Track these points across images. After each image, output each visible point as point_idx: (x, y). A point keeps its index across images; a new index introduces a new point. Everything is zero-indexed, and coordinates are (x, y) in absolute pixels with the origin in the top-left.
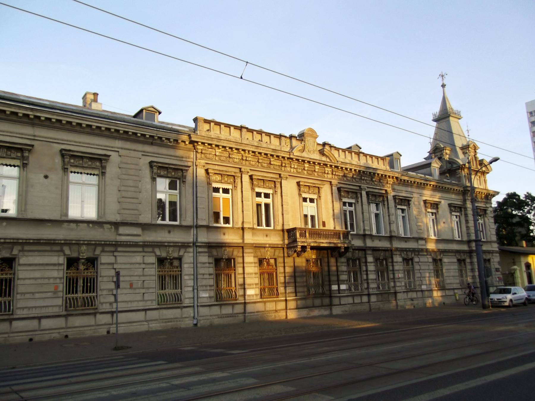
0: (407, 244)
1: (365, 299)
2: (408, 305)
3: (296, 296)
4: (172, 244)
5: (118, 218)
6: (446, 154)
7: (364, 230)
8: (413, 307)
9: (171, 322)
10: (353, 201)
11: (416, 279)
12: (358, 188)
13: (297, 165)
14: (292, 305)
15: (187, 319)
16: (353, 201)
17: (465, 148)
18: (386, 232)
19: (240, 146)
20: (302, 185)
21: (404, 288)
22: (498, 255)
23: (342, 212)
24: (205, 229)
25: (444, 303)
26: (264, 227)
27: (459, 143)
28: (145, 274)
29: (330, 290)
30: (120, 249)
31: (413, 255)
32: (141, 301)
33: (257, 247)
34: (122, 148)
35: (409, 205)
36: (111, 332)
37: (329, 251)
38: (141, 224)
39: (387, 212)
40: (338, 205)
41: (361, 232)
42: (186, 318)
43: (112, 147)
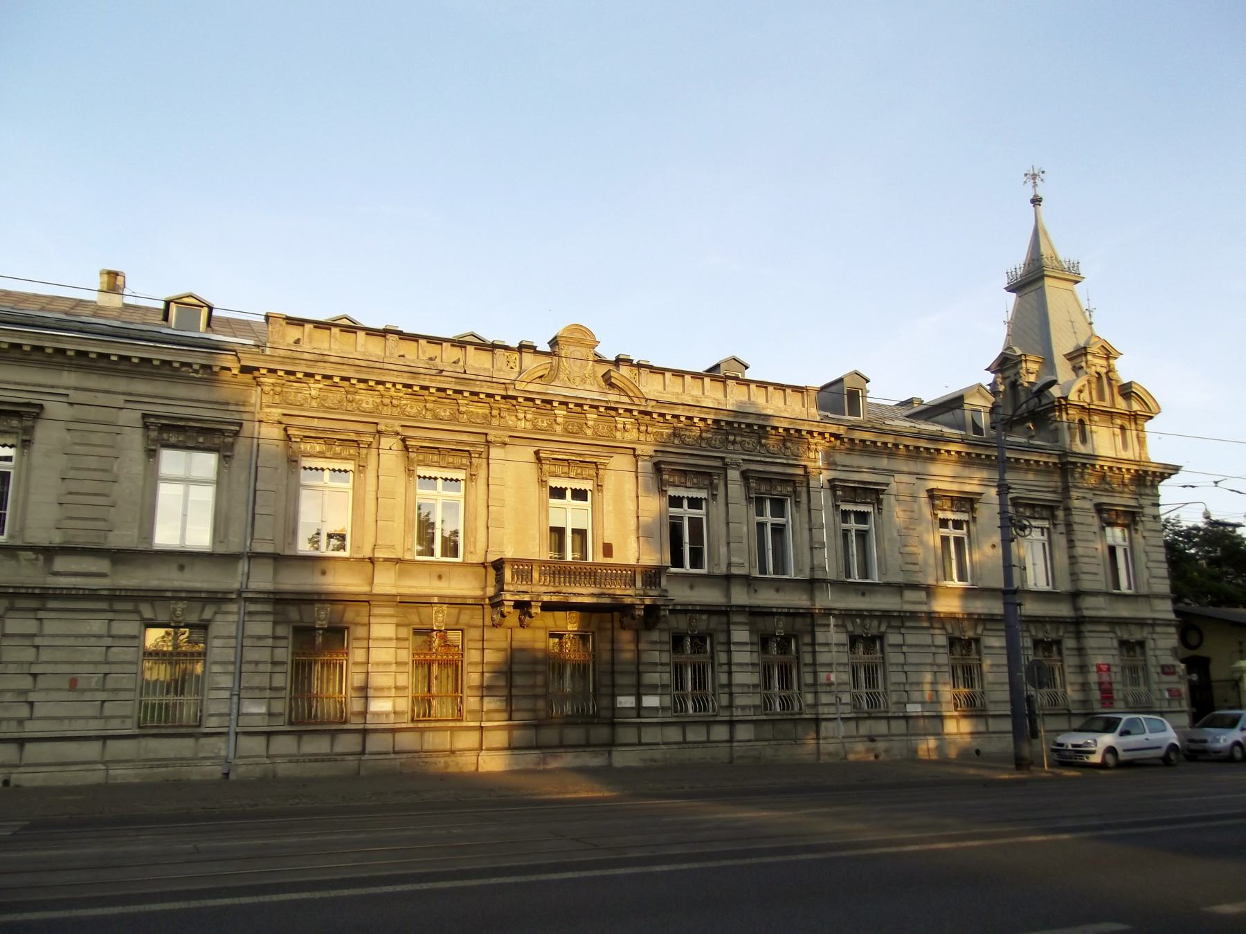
0: (867, 599)
1: (720, 733)
2: (859, 752)
3: (510, 719)
4: (183, 595)
5: (57, 539)
6: (1028, 372)
7: (729, 565)
8: (872, 758)
9: (166, 766)
10: (702, 494)
11: (890, 688)
12: (718, 464)
13: (534, 413)
14: (499, 738)
15: (208, 763)
16: (702, 494)
17: (1078, 356)
18: (799, 570)
19: (369, 373)
20: (547, 459)
21: (848, 709)
22: (1173, 630)
23: (667, 522)
24: (270, 561)
25: (978, 752)
26: (687, 568)
27: (1062, 345)
28: (111, 659)
29: (613, 707)
30: (51, 605)
31: (883, 629)
32: (96, 718)
33: (406, 602)
34: (76, 389)
35: (879, 502)
36: (12, 783)
37: (616, 614)
38: (109, 550)
39: (805, 519)
40: (653, 505)
41: (723, 570)
42: (205, 758)
43: (52, 387)
